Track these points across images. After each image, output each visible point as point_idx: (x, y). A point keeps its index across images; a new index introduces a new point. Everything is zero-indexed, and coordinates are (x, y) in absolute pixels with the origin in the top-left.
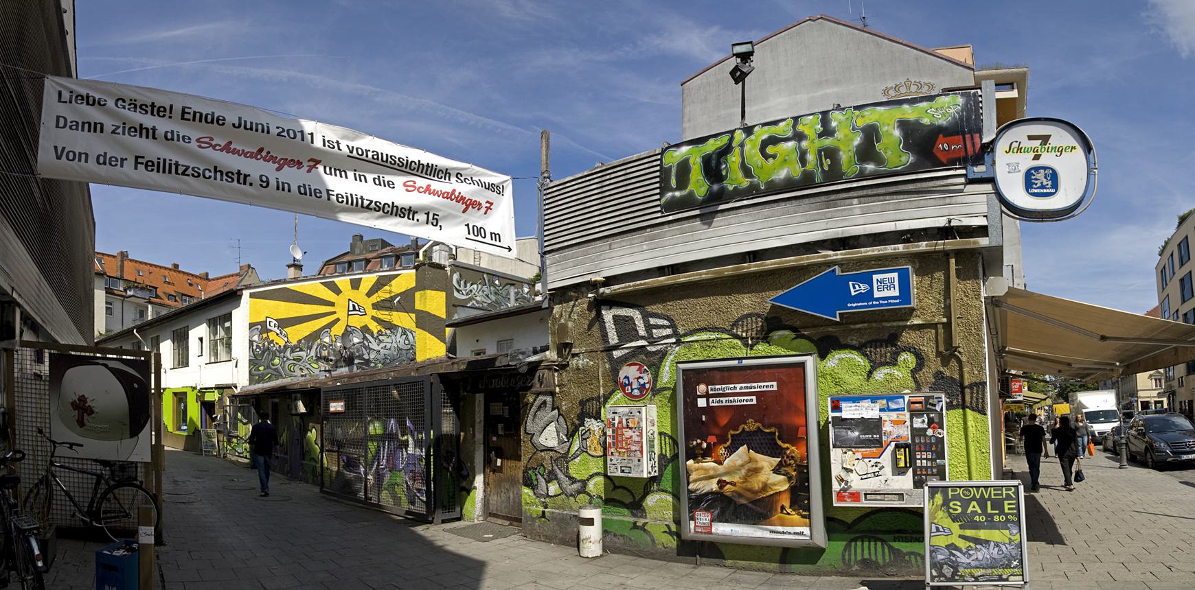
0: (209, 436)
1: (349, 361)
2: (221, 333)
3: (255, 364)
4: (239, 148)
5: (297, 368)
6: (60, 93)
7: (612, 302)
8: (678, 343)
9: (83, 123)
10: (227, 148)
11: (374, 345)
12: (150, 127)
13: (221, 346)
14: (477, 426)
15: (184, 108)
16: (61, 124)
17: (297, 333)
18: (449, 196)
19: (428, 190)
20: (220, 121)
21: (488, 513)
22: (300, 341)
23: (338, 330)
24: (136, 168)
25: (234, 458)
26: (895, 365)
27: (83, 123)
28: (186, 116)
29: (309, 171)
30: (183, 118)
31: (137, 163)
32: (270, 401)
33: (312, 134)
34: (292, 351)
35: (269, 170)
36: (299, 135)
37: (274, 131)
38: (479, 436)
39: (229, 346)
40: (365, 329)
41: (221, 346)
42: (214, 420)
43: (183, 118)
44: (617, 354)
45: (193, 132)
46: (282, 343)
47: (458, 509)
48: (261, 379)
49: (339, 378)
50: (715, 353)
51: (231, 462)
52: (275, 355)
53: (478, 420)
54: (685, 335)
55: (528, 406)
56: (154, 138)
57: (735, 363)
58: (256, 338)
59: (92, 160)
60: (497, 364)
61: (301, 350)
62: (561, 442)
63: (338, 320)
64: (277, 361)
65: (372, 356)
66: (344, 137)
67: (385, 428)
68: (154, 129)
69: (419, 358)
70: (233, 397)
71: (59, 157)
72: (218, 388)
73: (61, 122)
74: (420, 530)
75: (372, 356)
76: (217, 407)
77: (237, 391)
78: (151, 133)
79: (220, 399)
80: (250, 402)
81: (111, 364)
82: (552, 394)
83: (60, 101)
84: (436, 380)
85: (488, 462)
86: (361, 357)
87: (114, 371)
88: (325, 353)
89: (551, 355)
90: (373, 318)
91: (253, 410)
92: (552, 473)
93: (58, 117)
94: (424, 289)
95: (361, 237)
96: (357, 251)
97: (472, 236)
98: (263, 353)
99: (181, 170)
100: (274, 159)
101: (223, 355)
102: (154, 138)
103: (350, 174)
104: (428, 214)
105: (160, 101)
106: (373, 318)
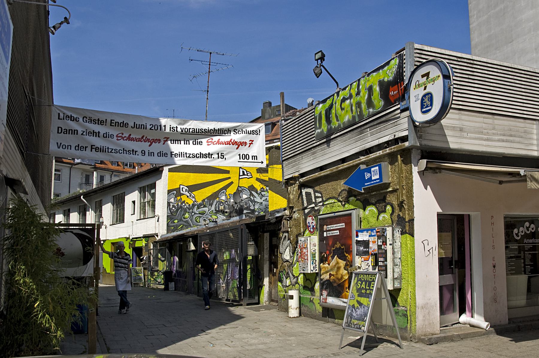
0: (137, 273)
1: (240, 212)
2: (148, 197)
3: (171, 219)
4: (134, 137)
5: (201, 220)
6: (59, 114)
7: (302, 186)
8: (323, 205)
9: (69, 130)
10: (129, 138)
11: (258, 199)
12: (97, 132)
13: (147, 208)
14: (265, 251)
15: (111, 120)
16: (60, 132)
17: (201, 195)
18: (228, 143)
19: (219, 143)
20: (125, 125)
21: (271, 299)
22: (204, 200)
23: (232, 190)
24: (91, 151)
25: (155, 286)
26: (385, 212)
27: (69, 130)
28: (112, 124)
29: (164, 144)
30: (111, 125)
31: (92, 148)
32: (178, 243)
33: (165, 126)
34: (198, 208)
35: (145, 146)
36: (159, 127)
37: (149, 127)
38: (266, 256)
39: (153, 206)
40: (252, 188)
41: (147, 208)
42: (142, 260)
43: (111, 125)
44: (306, 211)
45: (114, 131)
46: (191, 202)
47: (257, 298)
48: (176, 229)
49: (209, 228)
50: (334, 210)
51: (153, 289)
52: (185, 212)
53: (265, 248)
54: (326, 201)
55: (280, 239)
56: (99, 137)
57: (333, 215)
58: (172, 200)
59: (73, 148)
60: (266, 218)
61: (205, 206)
62: (291, 257)
63: (232, 183)
64: (187, 215)
65: (256, 207)
66: (180, 124)
67: (230, 255)
68: (99, 133)
69: (270, 209)
70: (155, 243)
71: (59, 148)
72: (146, 237)
73: (60, 130)
74: (231, 309)
75: (256, 207)
76: (144, 251)
77: (158, 239)
78: (96, 134)
79: (146, 245)
80: (171, 246)
81: (75, 231)
82: (288, 232)
83: (59, 119)
84: (244, 227)
85: (271, 271)
86: (248, 208)
87: (77, 235)
88: (222, 208)
89: (287, 212)
90: (258, 179)
91: (167, 251)
92: (288, 273)
93: (58, 128)
94: (272, 165)
95: (270, 103)
96: (267, 116)
97: (242, 160)
98: (177, 210)
99: (110, 150)
100: (148, 140)
101: (149, 213)
102: (99, 137)
103: (182, 142)
104: (218, 154)
105: (102, 118)
106: (258, 179)
